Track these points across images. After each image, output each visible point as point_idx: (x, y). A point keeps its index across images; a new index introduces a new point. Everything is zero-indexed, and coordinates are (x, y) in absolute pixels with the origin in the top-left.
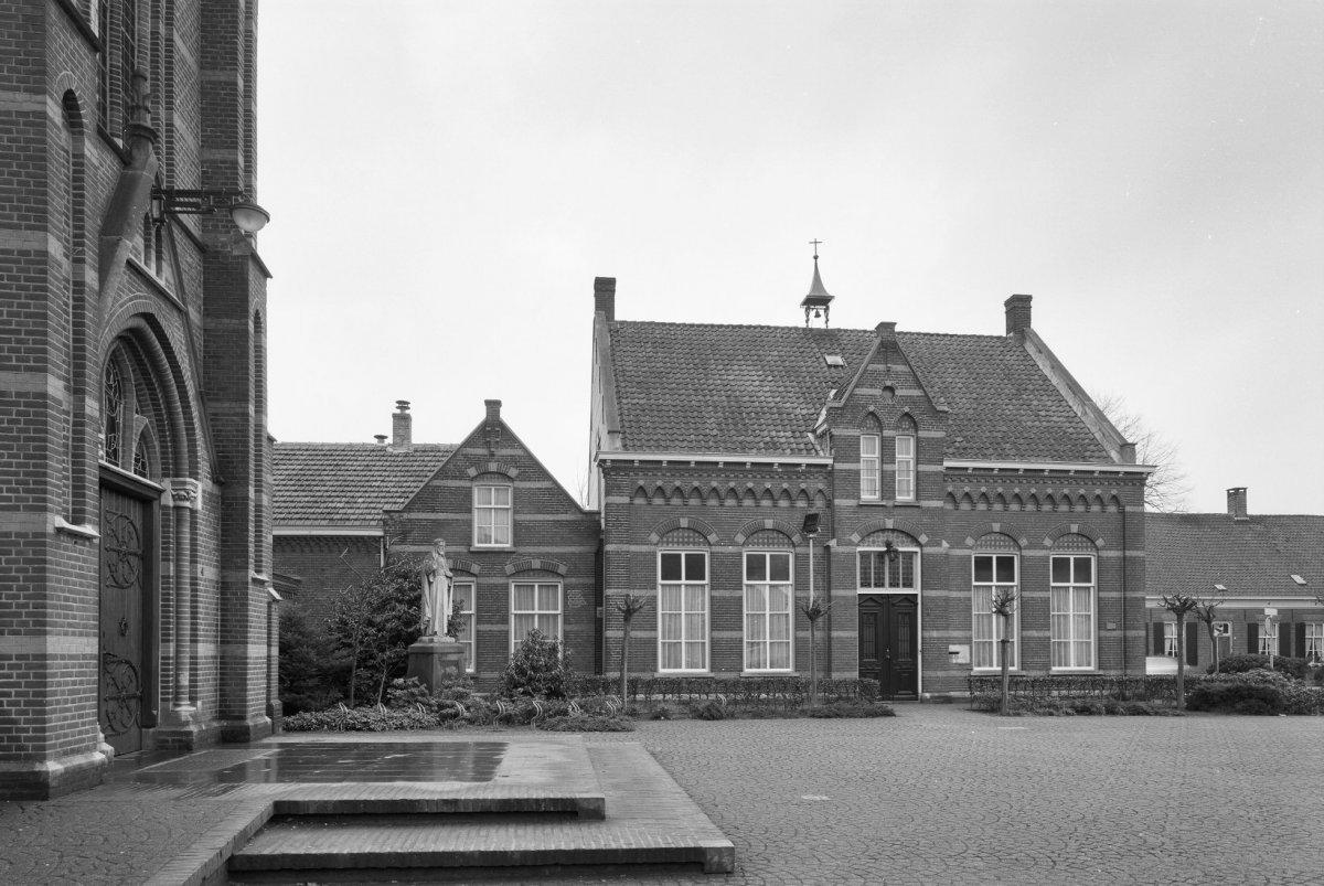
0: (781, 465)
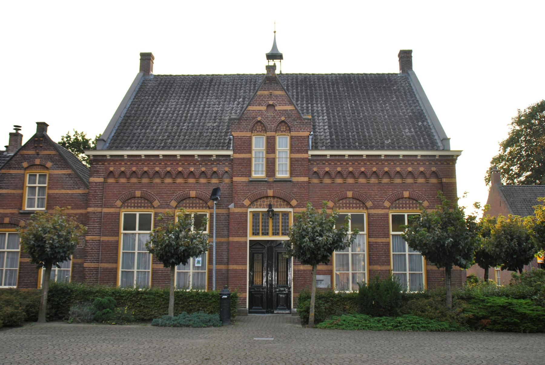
0: (199, 156)
